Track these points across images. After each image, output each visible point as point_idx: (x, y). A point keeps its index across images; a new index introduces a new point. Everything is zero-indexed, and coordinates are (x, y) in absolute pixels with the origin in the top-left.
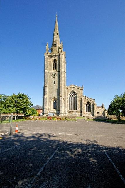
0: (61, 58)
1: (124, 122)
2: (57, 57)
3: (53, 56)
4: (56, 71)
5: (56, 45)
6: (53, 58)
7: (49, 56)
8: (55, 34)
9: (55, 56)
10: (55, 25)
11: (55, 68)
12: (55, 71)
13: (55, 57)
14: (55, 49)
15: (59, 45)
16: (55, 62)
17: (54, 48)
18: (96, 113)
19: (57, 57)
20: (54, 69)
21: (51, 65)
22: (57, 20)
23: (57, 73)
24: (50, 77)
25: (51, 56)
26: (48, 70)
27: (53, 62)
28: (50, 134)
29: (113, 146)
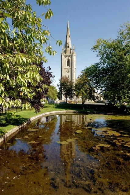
0: (74, 59)
1: (129, 137)
2: (70, 57)
3: (68, 56)
4: (69, 67)
5: (68, 47)
6: (67, 58)
7: (64, 56)
8: (68, 37)
9: (69, 56)
10: (68, 29)
11: (68, 65)
12: (69, 67)
13: (68, 57)
14: (68, 50)
15: (70, 47)
16: (68, 60)
17: (67, 48)
18: (49, 121)
19: (70, 57)
20: (68, 66)
21: (66, 63)
22: (69, 24)
23: (70, 69)
24: (65, 72)
25: (66, 56)
26: (63, 67)
27: (67, 61)
28: (53, 107)
29: (98, 115)
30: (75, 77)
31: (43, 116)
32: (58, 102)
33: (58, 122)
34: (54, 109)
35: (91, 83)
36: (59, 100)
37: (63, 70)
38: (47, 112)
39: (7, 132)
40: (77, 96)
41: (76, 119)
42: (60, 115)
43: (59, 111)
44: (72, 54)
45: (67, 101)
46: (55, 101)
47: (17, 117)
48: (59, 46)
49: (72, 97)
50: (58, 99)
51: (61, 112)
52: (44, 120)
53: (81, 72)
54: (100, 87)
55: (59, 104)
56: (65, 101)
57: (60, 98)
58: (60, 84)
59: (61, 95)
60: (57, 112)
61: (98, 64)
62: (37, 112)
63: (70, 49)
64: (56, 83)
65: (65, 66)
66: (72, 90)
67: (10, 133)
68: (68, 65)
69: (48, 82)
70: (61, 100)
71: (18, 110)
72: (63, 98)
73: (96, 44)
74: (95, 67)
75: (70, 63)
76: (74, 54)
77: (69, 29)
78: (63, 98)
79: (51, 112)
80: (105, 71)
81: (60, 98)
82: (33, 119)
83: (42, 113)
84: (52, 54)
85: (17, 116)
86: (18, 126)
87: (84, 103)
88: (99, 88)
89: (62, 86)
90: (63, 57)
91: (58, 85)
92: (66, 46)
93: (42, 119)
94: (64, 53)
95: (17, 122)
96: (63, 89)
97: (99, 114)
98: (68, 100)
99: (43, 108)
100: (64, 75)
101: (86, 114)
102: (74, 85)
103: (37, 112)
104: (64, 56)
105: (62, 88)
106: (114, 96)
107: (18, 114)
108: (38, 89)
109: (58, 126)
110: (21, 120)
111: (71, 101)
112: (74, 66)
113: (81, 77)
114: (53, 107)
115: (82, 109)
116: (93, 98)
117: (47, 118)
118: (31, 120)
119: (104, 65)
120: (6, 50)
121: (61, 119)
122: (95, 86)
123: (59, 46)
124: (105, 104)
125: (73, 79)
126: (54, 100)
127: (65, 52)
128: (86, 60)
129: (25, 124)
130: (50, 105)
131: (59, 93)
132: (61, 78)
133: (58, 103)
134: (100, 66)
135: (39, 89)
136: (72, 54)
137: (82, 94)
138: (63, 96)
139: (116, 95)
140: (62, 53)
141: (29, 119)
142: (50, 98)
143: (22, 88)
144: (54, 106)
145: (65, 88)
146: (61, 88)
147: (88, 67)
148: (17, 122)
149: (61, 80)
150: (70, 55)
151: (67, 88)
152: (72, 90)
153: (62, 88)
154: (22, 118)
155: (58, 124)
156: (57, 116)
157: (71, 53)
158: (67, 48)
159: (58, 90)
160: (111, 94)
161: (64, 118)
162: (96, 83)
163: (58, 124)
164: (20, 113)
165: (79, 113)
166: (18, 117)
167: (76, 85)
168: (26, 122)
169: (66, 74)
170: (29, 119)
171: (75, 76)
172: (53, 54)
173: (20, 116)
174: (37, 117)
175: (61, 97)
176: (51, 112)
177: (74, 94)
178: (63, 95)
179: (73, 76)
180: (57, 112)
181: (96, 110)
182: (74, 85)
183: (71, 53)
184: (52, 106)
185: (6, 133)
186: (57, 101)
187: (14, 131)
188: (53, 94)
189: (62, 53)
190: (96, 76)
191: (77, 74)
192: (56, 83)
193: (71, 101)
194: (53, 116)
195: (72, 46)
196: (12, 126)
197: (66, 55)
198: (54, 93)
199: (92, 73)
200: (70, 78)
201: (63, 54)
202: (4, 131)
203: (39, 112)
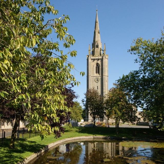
0: (105, 63)
2: (100, 60)
3: (96, 59)
5: (97, 46)
6: (96, 61)
7: (92, 59)
8: (97, 33)
9: (98, 59)
10: (96, 22)
11: (98, 72)
13: (97, 61)
15: (100, 46)
16: (97, 65)
17: (96, 49)
19: (100, 60)
20: (96, 73)
21: (94, 69)
22: (97, 16)
23: (100, 78)
25: (94, 60)
27: (95, 66)
28: (77, 131)
30: (108, 88)
31: (63, 144)
32: (83, 124)
33: (84, 152)
34: (77, 134)
35: (127, 98)
36: (84, 121)
37: (90, 78)
38: (69, 137)
39: (26, 159)
40: (109, 116)
41: (108, 147)
42: (86, 143)
43: (84, 137)
44: (102, 56)
45: (95, 123)
46: (79, 123)
47: (33, 143)
48: (83, 76)
49: (102, 118)
50: (82, 120)
51: (87, 137)
52: (63, 149)
53: (114, 84)
54: (140, 104)
55: (84, 127)
56: (93, 122)
57: (86, 119)
58: (85, 99)
59: (88, 115)
60: (81, 137)
61: (137, 73)
62: (57, 138)
63: (100, 49)
64: (80, 98)
65: (93, 73)
66: (102, 108)
67: (29, 160)
68: (96, 71)
69: (70, 103)
70: (87, 120)
71: (32, 135)
72: (90, 118)
73: (134, 45)
74: (134, 75)
75: (99, 69)
76: (106, 56)
77: (98, 22)
78: (90, 118)
79: (73, 138)
80: (146, 82)
81: (86, 119)
82: (51, 145)
83: (61, 139)
84: (77, 84)
85: (32, 142)
86: (35, 152)
87: (118, 125)
88: (138, 105)
89: (88, 102)
90: (90, 60)
91: (83, 101)
92: (95, 45)
93: (61, 148)
94: (91, 56)
95: (34, 148)
96: (90, 107)
97: (138, 141)
98: (97, 121)
99: (65, 133)
100: (91, 87)
101: (121, 140)
102: (105, 99)
103: (57, 138)
104: (92, 59)
105: (89, 106)
106: (158, 116)
107: (32, 139)
108: (62, 113)
109: (84, 158)
110: (38, 147)
111: (101, 122)
112: (106, 73)
113: (114, 91)
114: (77, 131)
115: (115, 134)
116: (133, 119)
117: (68, 145)
118: (49, 148)
119: (145, 73)
120: (64, 118)
121: (87, 148)
122: (133, 102)
123: (83, 76)
124: (148, 127)
125: (104, 91)
126: (78, 121)
127: (93, 53)
128: (121, 65)
129: (43, 151)
130: (73, 129)
131: (84, 111)
132: (88, 91)
133: (83, 126)
134: (139, 74)
135: (63, 113)
136: (103, 57)
137: (115, 113)
138: (89, 116)
139: (161, 115)
140: (88, 56)
141: (47, 146)
142: (72, 119)
143: (52, 114)
144: (78, 130)
145: (92, 105)
146: (86, 106)
147: (125, 75)
148: (34, 148)
149: (87, 94)
150: (100, 58)
151: (95, 105)
152: (102, 108)
153: (89, 106)
154: (39, 145)
155: (82, 155)
156: (82, 144)
157: (101, 55)
158: (96, 49)
159: (83, 107)
160: (154, 114)
161: (91, 146)
162: (134, 98)
163: (82, 155)
164: (34, 138)
165: (111, 139)
166: (33, 144)
167: (107, 100)
168: (43, 150)
169: (95, 86)
170: (47, 146)
171: (106, 88)
172: (78, 84)
173: (36, 143)
174: (55, 144)
175: (88, 117)
176: (73, 138)
177: (105, 113)
178: (89, 114)
179: (104, 87)
180: (81, 137)
181: (134, 135)
182: (105, 99)
183: (101, 55)
184: (75, 129)
185: (25, 159)
186: (82, 123)
187: (33, 158)
188: (76, 113)
189: (88, 56)
190: (135, 88)
191: (110, 84)
192: (80, 98)
193: (101, 122)
194: (77, 143)
195: (102, 45)
196: (29, 153)
197: (94, 58)
198: (78, 111)
199: (128, 83)
200: (99, 91)
201: (89, 58)
202: (22, 157)
203: (59, 137)
